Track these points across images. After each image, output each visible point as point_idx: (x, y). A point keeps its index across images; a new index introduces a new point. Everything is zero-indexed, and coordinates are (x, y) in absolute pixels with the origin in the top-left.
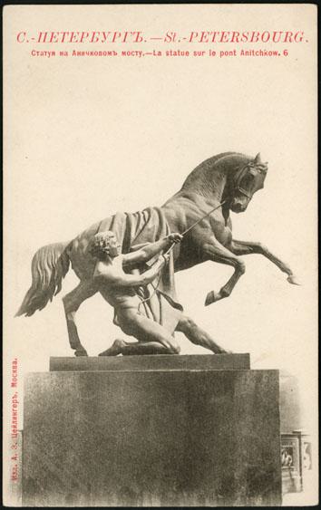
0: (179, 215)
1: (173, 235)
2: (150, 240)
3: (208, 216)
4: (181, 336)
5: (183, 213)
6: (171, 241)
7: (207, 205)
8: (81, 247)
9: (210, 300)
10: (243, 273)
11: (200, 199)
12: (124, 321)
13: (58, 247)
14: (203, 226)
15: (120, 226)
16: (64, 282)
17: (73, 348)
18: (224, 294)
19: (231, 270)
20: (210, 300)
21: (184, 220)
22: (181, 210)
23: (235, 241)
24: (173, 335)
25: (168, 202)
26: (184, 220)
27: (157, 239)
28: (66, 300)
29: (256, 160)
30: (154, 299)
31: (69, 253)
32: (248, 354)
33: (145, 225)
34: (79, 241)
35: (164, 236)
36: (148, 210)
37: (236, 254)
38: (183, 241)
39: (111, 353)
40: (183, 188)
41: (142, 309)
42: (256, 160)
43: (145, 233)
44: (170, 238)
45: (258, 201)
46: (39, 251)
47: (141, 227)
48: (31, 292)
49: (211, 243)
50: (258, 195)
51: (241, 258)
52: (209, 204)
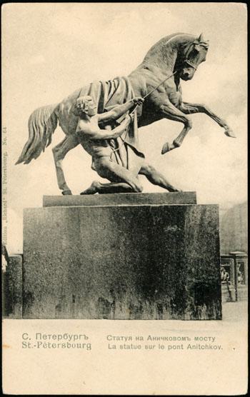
2: (118, 103)
4: (143, 178)
6: (135, 103)
11: (157, 69)
16: (53, 136)
22: (144, 80)
28: (55, 151)
31: (57, 113)
34: (65, 104)
37: (184, 115)
47: (112, 92)
51: (189, 117)
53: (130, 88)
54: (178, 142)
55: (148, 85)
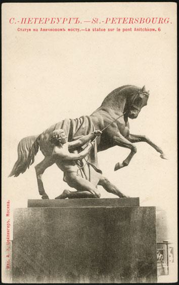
0: (100, 120)
1: (96, 131)
2: (84, 134)
3: (116, 121)
4: (101, 188)
5: (102, 119)
6: (95, 135)
7: (115, 115)
8: (45, 138)
9: (117, 168)
10: (135, 152)
11: (112, 111)
12: (69, 179)
13: (33, 138)
14: (113, 126)
15: (67, 126)
16: (36, 157)
17: (41, 194)
18: (125, 164)
19: (129, 151)
20: (117, 168)
21: (103, 123)
22: (101, 117)
23: (131, 135)
24: (96, 187)
25: (94, 113)
26: (103, 123)
27: (88, 133)
28: (37, 168)
29: (143, 89)
30: (86, 167)
31: (38, 141)
32: (138, 198)
33: (81, 125)
34: (44, 135)
35: (91, 132)
36: (83, 117)
37: (132, 142)
38: (102, 135)
39: (62, 197)
40: (102, 105)
41: (79, 173)
42: (143, 89)
43: (81, 130)
44: (95, 133)
45: (144, 112)
46: (22, 140)
47: (78, 127)
48: (17, 163)
49: (117, 136)
50: (144, 109)
51: (135, 144)
52: (117, 114)
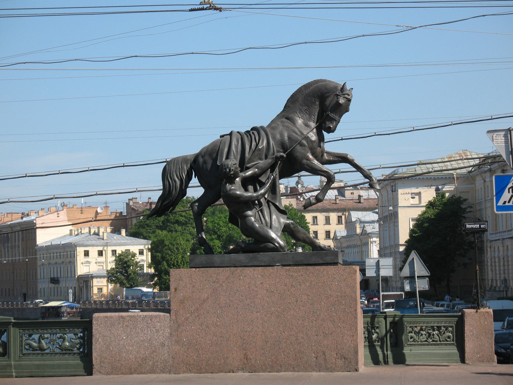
7: (305, 126)
13: (184, 159)
14: (301, 145)
29: (343, 89)
33: (257, 145)
44: (277, 158)
45: (346, 125)
49: (308, 159)
50: (345, 117)
53: (272, 142)
54: (320, 197)
55: (289, 138)
